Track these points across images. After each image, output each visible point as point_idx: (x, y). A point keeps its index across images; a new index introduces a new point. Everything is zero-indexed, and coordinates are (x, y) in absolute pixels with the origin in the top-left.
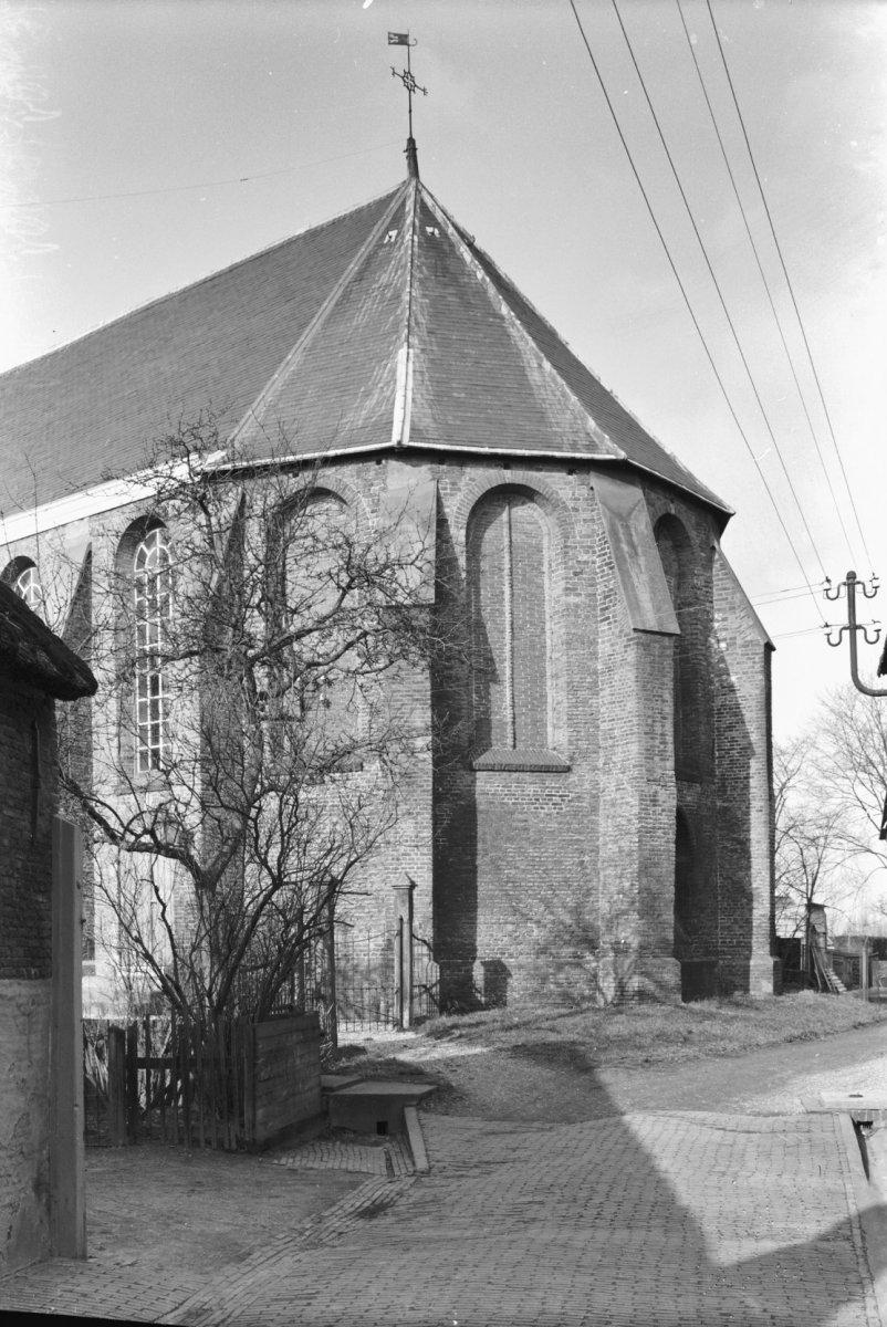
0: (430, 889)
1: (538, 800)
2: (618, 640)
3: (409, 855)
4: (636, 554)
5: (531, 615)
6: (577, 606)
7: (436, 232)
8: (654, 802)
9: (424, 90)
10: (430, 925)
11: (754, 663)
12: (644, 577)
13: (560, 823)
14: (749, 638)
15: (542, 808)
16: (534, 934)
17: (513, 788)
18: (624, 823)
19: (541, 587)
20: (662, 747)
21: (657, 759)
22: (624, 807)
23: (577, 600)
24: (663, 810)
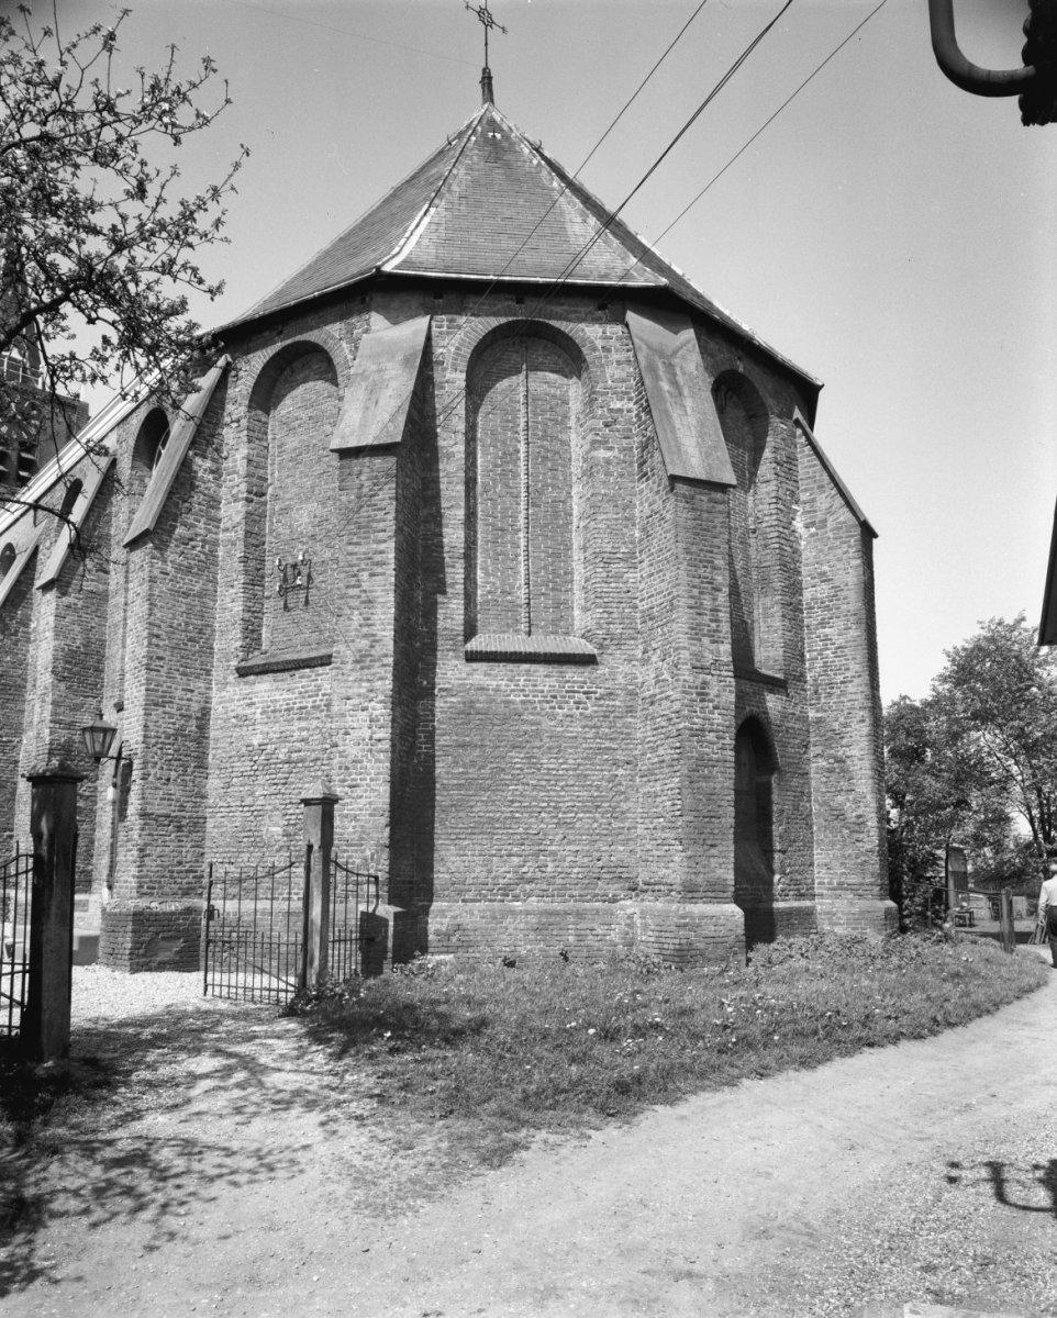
0: (387, 807)
1: (555, 697)
2: (657, 498)
3: (360, 762)
4: (681, 394)
5: (554, 478)
6: (608, 462)
7: (498, 136)
8: (703, 696)
9: (503, 28)
10: (385, 855)
11: (849, 547)
12: (692, 420)
13: (584, 727)
14: (842, 519)
15: (560, 708)
16: (549, 869)
17: (521, 683)
18: (664, 724)
19: (566, 443)
20: (714, 625)
21: (706, 640)
22: (664, 702)
23: (609, 454)
24: (716, 708)
